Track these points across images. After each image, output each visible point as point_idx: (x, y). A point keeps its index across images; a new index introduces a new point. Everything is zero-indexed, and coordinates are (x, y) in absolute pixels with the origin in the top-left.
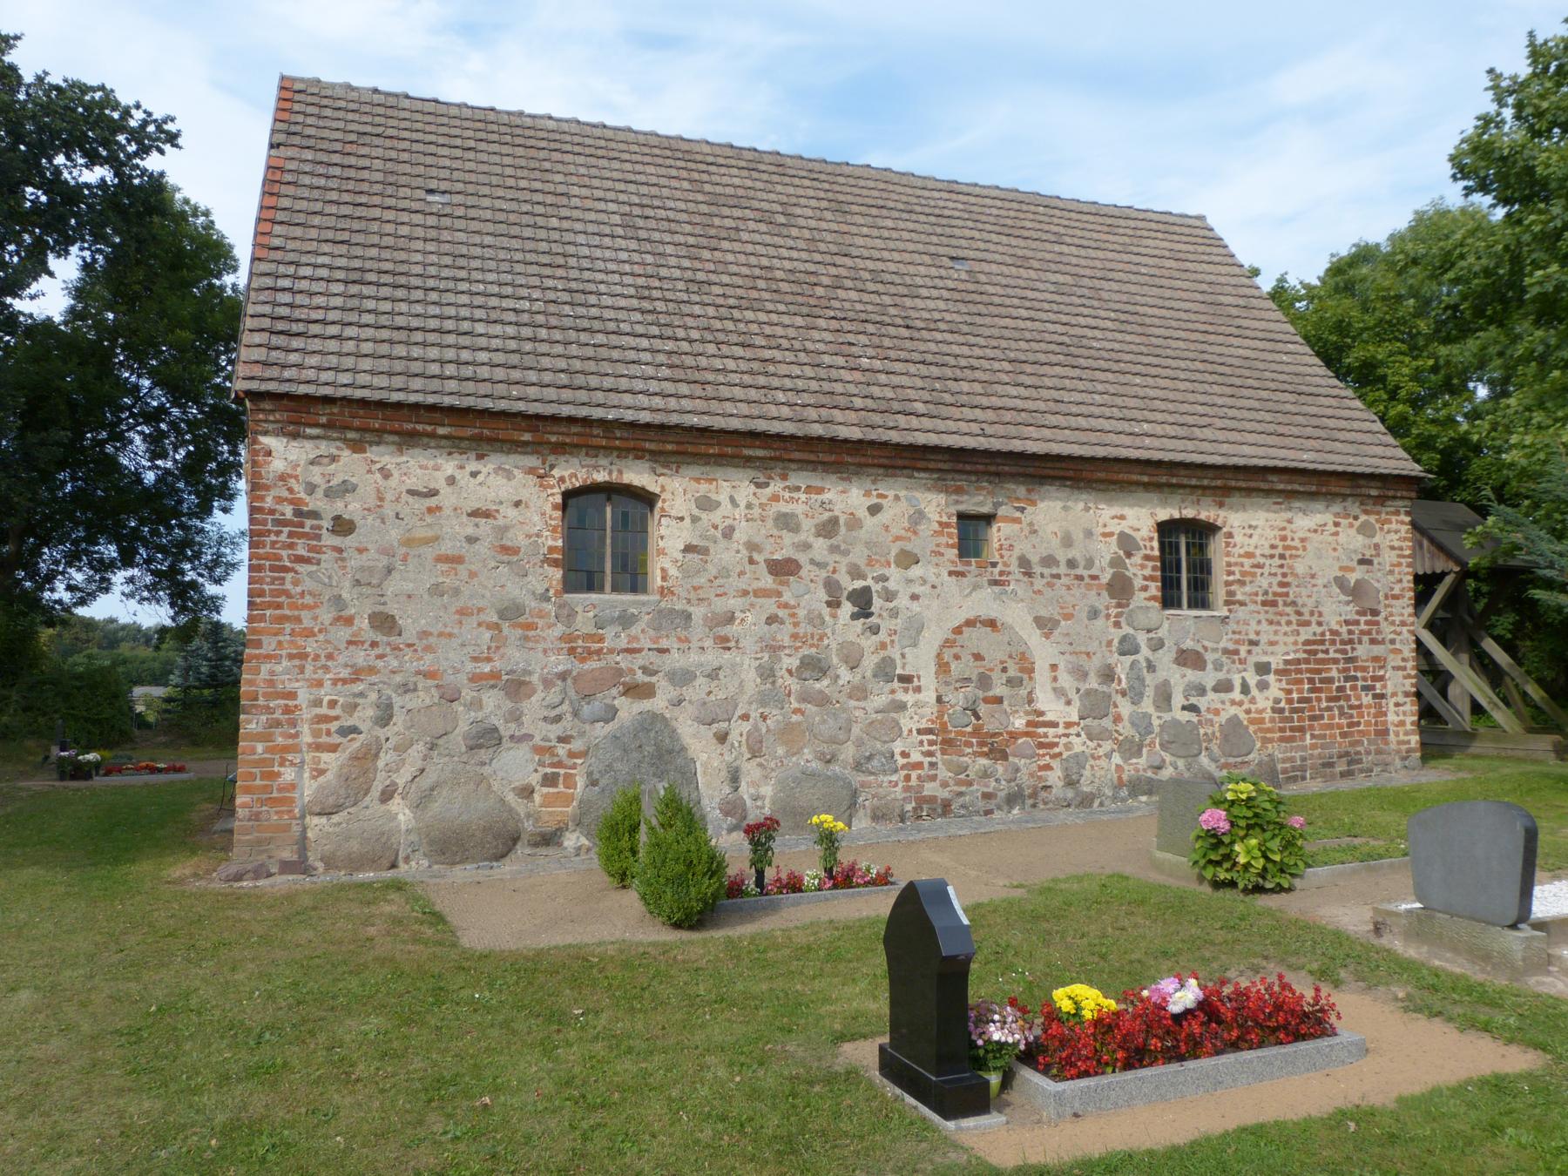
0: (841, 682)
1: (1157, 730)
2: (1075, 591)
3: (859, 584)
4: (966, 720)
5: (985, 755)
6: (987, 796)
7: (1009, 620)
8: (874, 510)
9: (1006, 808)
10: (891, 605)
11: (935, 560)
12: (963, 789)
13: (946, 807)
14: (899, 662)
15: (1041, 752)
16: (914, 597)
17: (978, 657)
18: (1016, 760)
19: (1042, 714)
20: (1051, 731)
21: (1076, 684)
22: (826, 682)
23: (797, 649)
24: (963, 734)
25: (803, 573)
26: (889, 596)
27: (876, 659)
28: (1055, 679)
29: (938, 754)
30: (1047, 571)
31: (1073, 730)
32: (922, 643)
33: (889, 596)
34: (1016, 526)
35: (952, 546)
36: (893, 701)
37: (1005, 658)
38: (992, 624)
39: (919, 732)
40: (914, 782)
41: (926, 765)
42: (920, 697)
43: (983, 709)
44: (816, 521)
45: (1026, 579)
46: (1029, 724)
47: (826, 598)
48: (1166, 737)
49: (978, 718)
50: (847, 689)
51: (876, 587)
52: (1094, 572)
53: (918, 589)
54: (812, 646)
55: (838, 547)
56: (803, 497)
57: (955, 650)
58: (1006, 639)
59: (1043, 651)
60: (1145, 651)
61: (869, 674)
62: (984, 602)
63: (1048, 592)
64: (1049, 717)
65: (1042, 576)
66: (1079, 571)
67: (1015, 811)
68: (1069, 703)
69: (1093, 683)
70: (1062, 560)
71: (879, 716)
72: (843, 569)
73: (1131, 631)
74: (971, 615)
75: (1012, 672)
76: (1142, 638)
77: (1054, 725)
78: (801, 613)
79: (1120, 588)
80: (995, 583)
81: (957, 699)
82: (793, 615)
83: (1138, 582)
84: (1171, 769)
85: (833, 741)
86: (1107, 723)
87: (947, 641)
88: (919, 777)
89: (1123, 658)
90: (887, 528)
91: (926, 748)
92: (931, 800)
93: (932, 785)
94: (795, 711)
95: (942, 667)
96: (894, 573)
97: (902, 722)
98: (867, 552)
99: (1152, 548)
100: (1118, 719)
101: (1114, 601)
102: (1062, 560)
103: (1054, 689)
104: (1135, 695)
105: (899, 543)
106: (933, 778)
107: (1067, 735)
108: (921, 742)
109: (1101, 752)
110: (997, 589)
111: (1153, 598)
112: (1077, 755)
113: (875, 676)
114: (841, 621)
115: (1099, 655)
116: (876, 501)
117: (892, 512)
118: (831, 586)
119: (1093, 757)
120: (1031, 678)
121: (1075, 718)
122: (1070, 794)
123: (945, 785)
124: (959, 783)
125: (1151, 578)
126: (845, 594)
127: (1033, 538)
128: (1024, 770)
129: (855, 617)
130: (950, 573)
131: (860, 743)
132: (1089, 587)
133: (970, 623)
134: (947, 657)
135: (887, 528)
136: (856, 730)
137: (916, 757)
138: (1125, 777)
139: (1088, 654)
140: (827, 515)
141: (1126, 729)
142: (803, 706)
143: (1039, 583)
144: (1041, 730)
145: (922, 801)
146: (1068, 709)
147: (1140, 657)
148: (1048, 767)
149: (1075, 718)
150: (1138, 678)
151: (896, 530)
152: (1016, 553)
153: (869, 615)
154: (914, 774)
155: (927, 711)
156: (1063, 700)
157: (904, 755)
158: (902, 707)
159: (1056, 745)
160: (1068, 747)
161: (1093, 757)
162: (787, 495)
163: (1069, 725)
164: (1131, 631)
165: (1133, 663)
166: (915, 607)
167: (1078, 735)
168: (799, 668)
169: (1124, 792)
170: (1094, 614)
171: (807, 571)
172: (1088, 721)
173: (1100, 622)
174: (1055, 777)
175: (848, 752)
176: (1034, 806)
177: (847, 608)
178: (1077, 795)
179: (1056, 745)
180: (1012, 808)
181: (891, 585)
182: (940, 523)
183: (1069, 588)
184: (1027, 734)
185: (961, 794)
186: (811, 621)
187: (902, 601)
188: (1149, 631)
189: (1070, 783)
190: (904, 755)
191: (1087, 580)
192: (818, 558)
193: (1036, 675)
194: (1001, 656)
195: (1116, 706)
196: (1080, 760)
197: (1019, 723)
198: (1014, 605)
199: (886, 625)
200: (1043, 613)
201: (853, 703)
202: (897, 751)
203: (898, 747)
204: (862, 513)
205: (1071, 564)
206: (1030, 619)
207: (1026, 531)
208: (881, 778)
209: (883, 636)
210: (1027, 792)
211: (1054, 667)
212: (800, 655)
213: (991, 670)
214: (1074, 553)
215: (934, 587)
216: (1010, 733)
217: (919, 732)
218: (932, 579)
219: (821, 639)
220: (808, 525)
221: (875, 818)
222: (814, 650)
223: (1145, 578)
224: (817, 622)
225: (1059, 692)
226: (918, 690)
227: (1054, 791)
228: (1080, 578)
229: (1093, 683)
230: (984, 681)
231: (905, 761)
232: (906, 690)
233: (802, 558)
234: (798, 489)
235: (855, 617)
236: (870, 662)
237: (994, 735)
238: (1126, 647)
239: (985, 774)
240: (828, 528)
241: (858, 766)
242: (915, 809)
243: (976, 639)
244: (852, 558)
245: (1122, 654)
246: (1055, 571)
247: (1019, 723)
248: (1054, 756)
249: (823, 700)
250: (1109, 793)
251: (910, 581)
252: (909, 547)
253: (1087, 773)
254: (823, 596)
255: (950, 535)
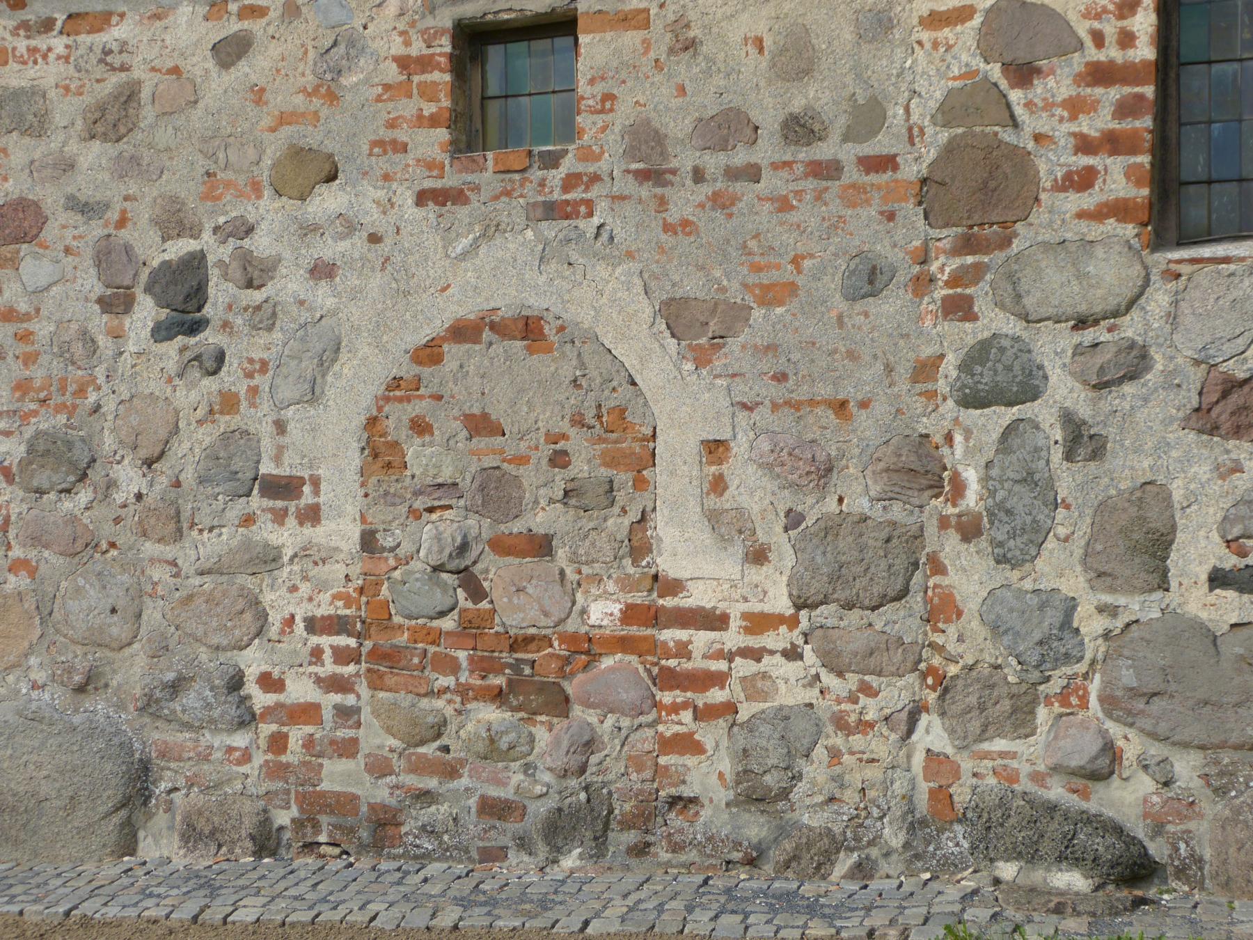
0: (119, 497)
1: (1093, 649)
2: (807, 214)
3: (179, 248)
4: (440, 600)
5: (498, 696)
6: (493, 809)
7: (581, 314)
8: (231, 51)
9: (542, 850)
10: (257, 296)
11: (381, 164)
12: (432, 783)
13: (384, 825)
14: (267, 445)
15: (667, 697)
16: (322, 271)
17: (480, 425)
18: (592, 717)
19: (675, 587)
20: (701, 639)
21: (786, 500)
22: (84, 496)
23: (26, 417)
24: (436, 637)
25: (50, 232)
26: (253, 274)
27: (206, 436)
28: (718, 485)
29: (363, 689)
30: (713, 162)
31: (771, 640)
32: (330, 393)
33: (253, 274)
34: (631, 38)
35: (433, 121)
36: (247, 544)
37: (565, 426)
38: (529, 329)
39: (313, 625)
40: (294, 752)
41: (327, 714)
42: (318, 534)
43: (495, 571)
44: (87, 99)
45: (646, 191)
46: (630, 614)
47: (99, 290)
48: (1128, 677)
49: (477, 593)
50: (132, 516)
51: (218, 252)
52: (880, 145)
53: (329, 249)
54: (59, 408)
55: (135, 160)
56: (59, 44)
57: (418, 408)
58: (568, 370)
59: (681, 404)
60: (1064, 390)
61: (188, 477)
62: (500, 267)
63: (714, 226)
64: (698, 597)
65: (698, 176)
66: (824, 151)
67: (570, 861)
68: (758, 556)
69: (858, 494)
70: (768, 116)
71: (208, 582)
72: (143, 213)
73: (1010, 326)
74: (468, 309)
75: (580, 467)
76: (1053, 348)
77: (714, 621)
78: (43, 329)
79: (979, 191)
80: (553, 211)
81: (430, 538)
82: (25, 337)
83: (1053, 163)
84: (1145, 784)
85: (95, 641)
86: (901, 620)
87: (397, 382)
88: (309, 743)
89: (973, 416)
90: (258, 95)
91: (329, 667)
92: (343, 804)
93: (344, 765)
94: (16, 566)
95: (381, 454)
96: (270, 214)
97: (268, 598)
98: (202, 164)
99: (1127, 39)
100: (942, 610)
101: (947, 236)
102: (768, 116)
103: (713, 518)
104: (1012, 533)
105: (286, 131)
106: (348, 749)
107: (755, 655)
108: (317, 653)
109: (872, 709)
110: (550, 229)
111: (1118, 210)
112: (783, 715)
113: (202, 481)
114: (131, 347)
115: (881, 408)
116: (234, 26)
117: (275, 50)
118: (107, 256)
119: (840, 723)
120: (640, 484)
121: (780, 603)
122: (755, 828)
123: (379, 768)
124: (421, 767)
125: (1113, 143)
126: (144, 276)
127: (683, 69)
128: (612, 747)
129: (162, 332)
130: (422, 198)
131: (161, 650)
132: (855, 196)
133: (463, 332)
134: (397, 419)
135: (258, 95)
136: (153, 614)
137: (300, 690)
138: (961, 794)
139: (841, 407)
140: (115, 79)
141: (967, 643)
142: (32, 554)
143: (685, 200)
144: (670, 635)
145: (315, 805)
146: (756, 574)
147: (1044, 412)
148: (687, 744)
149: (780, 603)
150: (1028, 479)
151: (284, 98)
152: (624, 114)
153: (194, 328)
154: (296, 735)
155: (336, 571)
156: (738, 550)
157: (269, 683)
158: (269, 559)
159: (719, 679)
160: (755, 687)
161: (840, 723)
162: (22, 45)
163: (759, 623)
164: (1010, 326)
165: (1010, 430)
166: (323, 296)
167: (792, 654)
168: (24, 464)
169: (956, 840)
170: (870, 279)
171: (61, 226)
172: (827, 614)
173: (891, 306)
174: (708, 774)
175: (133, 671)
176: (641, 850)
177: (147, 311)
178: (782, 831)
179: (719, 679)
180: (557, 851)
181: (261, 244)
182: (404, 63)
183: (784, 205)
184: (624, 644)
185: (425, 797)
186: (64, 352)
187: (289, 285)
188: (1081, 323)
189: (753, 796)
190: (269, 683)
191: (852, 174)
192: (87, 193)
193: (660, 475)
194: (550, 418)
195: (938, 568)
196: (795, 734)
197: (602, 612)
198: (602, 270)
199: (243, 349)
200: (693, 286)
201: (150, 548)
202: (252, 673)
203: (253, 662)
204: (201, 64)
205: (800, 129)
206: (646, 310)
207: (660, 50)
208: (207, 737)
209: (231, 376)
210: (623, 808)
211: (715, 449)
212: (29, 432)
213: (521, 460)
214: (813, 95)
215: (374, 239)
216: (571, 639)
217: (313, 625)
218: (373, 218)
219: (81, 392)
220: (66, 111)
221: (191, 835)
222: (62, 419)
223: (1085, 145)
224: (78, 349)
225: (725, 525)
226: (312, 515)
227: (706, 813)
228: (826, 170)
229: (858, 494)
230: (496, 492)
231: (270, 699)
232: (280, 517)
233: (50, 197)
234: (47, 25)
235: (162, 332)
236: (194, 443)
237: (525, 642)
238: (985, 377)
239: (493, 750)
240: (114, 118)
241: (149, 706)
242: (298, 824)
243: (485, 376)
244: (171, 184)
245: (973, 400)
246: (740, 157)
247: (602, 612)
248: (704, 714)
249: (83, 546)
250: (894, 837)
251: (309, 230)
252: (313, 137)
253: (815, 771)
254: (91, 283)
255: (428, 92)
